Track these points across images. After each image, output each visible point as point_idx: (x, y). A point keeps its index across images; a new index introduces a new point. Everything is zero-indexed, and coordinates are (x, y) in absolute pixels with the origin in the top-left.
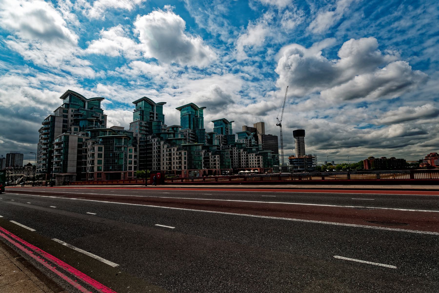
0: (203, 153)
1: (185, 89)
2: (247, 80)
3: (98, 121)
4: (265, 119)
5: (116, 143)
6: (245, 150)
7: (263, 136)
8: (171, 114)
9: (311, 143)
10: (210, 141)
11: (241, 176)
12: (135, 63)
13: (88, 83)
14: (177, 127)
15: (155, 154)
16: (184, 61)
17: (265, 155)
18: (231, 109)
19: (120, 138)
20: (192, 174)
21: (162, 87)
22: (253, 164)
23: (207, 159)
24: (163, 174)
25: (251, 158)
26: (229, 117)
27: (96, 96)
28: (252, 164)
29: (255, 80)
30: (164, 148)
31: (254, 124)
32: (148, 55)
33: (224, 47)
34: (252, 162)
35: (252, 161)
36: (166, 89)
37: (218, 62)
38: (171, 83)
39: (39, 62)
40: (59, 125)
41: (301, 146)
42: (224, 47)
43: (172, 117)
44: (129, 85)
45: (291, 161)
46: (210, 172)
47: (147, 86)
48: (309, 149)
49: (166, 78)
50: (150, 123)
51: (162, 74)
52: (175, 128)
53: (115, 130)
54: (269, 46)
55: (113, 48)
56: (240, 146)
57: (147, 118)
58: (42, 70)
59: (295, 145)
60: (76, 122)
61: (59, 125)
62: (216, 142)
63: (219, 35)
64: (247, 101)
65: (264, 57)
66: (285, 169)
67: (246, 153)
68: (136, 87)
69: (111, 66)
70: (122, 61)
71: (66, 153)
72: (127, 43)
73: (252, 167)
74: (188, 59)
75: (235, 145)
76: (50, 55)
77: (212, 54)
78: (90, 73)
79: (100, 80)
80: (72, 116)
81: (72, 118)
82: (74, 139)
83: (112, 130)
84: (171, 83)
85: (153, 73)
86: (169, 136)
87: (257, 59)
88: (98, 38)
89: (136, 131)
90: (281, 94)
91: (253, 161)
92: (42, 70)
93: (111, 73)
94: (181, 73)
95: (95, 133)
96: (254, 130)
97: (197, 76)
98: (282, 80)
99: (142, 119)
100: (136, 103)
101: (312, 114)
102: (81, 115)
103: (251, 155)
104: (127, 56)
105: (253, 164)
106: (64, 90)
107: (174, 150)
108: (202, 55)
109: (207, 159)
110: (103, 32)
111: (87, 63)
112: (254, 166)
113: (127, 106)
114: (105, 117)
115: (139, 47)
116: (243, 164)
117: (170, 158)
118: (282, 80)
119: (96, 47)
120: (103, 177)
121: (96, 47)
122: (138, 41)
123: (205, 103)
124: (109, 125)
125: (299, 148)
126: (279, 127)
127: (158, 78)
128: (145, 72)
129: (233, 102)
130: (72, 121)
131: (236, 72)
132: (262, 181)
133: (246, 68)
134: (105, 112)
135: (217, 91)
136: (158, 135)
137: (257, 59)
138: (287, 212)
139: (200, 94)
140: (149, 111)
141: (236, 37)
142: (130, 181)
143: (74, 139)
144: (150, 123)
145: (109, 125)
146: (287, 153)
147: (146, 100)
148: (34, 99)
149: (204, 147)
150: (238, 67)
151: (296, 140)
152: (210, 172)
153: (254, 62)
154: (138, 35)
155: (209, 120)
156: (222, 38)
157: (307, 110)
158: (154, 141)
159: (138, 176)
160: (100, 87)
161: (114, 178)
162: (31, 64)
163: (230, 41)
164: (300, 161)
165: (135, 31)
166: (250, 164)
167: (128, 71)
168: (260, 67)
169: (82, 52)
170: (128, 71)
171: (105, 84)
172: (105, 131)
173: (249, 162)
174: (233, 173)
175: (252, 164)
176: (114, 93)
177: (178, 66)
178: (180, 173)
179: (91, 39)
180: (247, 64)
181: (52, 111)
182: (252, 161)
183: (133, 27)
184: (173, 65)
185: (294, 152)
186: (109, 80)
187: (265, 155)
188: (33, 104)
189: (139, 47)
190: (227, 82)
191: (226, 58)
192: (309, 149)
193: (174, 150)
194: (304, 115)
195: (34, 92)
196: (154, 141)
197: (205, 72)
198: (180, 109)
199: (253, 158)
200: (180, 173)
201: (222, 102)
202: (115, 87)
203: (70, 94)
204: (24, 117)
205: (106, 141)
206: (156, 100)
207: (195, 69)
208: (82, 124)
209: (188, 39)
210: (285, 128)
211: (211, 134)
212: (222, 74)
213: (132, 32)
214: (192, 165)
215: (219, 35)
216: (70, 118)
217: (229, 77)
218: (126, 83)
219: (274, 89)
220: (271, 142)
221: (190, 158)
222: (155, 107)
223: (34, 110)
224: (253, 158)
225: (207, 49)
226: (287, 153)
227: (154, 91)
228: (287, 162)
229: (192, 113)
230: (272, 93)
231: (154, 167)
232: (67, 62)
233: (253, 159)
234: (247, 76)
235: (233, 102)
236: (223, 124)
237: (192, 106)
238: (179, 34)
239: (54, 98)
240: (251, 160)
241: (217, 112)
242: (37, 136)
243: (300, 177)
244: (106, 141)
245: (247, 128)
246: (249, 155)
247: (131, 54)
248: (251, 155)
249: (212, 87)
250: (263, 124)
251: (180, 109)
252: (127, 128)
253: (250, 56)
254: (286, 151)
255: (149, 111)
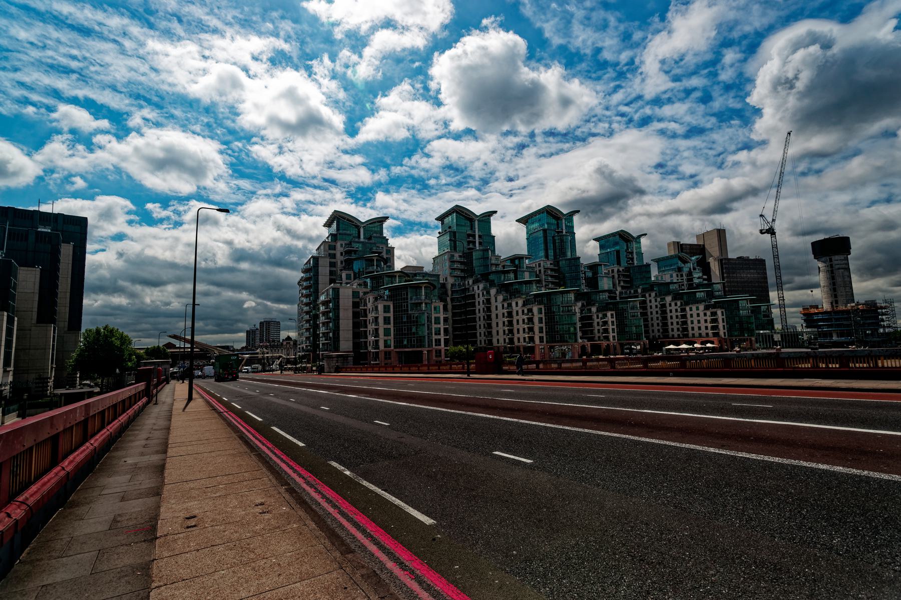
0: (577, 308)
1: (531, 178)
2: (674, 136)
3: (381, 259)
4: (725, 220)
5: (412, 299)
6: (677, 296)
7: (724, 262)
8: (508, 235)
9: (872, 271)
10: (593, 282)
11: (670, 356)
12: (436, 144)
13: (362, 194)
14: (520, 258)
15: (480, 315)
16: (528, 122)
17: (731, 308)
18: (636, 207)
19: (417, 287)
20: (557, 353)
21: (485, 182)
22: (700, 328)
23: (586, 320)
24: (498, 353)
25: (695, 315)
26: (633, 227)
27: (374, 214)
28: (696, 329)
29: (694, 132)
30: (498, 301)
31: (698, 236)
32: (458, 124)
33: (611, 73)
34: (696, 325)
35: (695, 322)
36: (495, 185)
37: (599, 111)
38: (503, 170)
39: (293, 171)
40: (324, 270)
41: (839, 280)
42: (611, 73)
43: (509, 238)
44: (426, 187)
45: (810, 318)
46: (596, 349)
47: (459, 185)
48: (863, 287)
49: (493, 163)
50: (468, 256)
51: (486, 156)
52: (517, 260)
53: (410, 273)
54: (727, 43)
55: (397, 125)
56: (663, 288)
57: (462, 245)
58: (296, 183)
59: (821, 278)
60: (348, 264)
61: (324, 270)
62: (605, 284)
63: (598, 50)
64: (675, 185)
65: (715, 74)
66: (791, 338)
67: (679, 303)
68: (441, 188)
69: (395, 159)
70: (414, 145)
71: (337, 318)
72: (421, 109)
73: (697, 335)
74: (537, 116)
75: (651, 287)
76: (306, 157)
77: (585, 94)
78: (364, 177)
79: (378, 186)
80: (342, 254)
81: (342, 258)
82: (346, 294)
83: (403, 273)
84: (503, 170)
85: (468, 158)
86: (507, 276)
87: (695, 82)
88: (372, 113)
89: (444, 272)
90: (773, 153)
91: (699, 322)
92: (296, 183)
93: (396, 170)
94: (522, 147)
95: (377, 281)
96: (699, 250)
97: (554, 147)
98: (771, 119)
99: (454, 247)
100: (441, 218)
101: (870, 192)
102: (355, 252)
103: (694, 308)
104: (422, 135)
105: (700, 328)
106: (328, 211)
107: (518, 305)
108: (566, 102)
109: (586, 320)
110: (382, 101)
111: (358, 159)
112: (704, 334)
113: (424, 227)
114: (391, 251)
115: (441, 112)
116: (674, 328)
117: (511, 320)
118: (771, 119)
119: (373, 129)
120: (394, 360)
121: (373, 129)
122: (438, 103)
123: (575, 202)
124: (399, 265)
125: (834, 284)
126: (767, 237)
127: (478, 165)
128: (454, 157)
129: (642, 192)
130: (342, 262)
131: (645, 122)
132: (727, 368)
133: (667, 110)
134: (392, 242)
135: (603, 172)
136: (485, 277)
137: (695, 82)
138: (679, 430)
139: (564, 184)
140: (466, 231)
141: (642, 44)
142: (438, 367)
143: (346, 294)
144: (468, 256)
145: (399, 265)
146: (795, 300)
147: (459, 212)
148: (290, 232)
149: (579, 296)
150: (648, 111)
151: (820, 265)
152: (596, 349)
153: (688, 92)
154: (438, 91)
155: (586, 237)
156: (607, 55)
157: (861, 182)
158: (478, 289)
159: (454, 356)
160: (381, 198)
161: (410, 361)
162: (283, 177)
163: (624, 57)
164: (837, 320)
165: (433, 85)
166: (693, 329)
167: (424, 163)
168: (706, 99)
169: (351, 142)
170: (424, 163)
171: (387, 191)
172: (392, 276)
173: (690, 326)
174: (649, 349)
175: (696, 329)
176: (404, 206)
177: (514, 133)
178: (531, 350)
179: (361, 119)
180: (670, 101)
181: (313, 249)
182: (695, 322)
183: (428, 78)
184: (506, 134)
185: (819, 296)
186: (394, 184)
187: (731, 308)
188: (288, 240)
189: (441, 112)
190: (624, 149)
191: (618, 97)
192: (863, 287)
193: (518, 305)
194: (845, 197)
195: (288, 221)
196: (478, 289)
197: (572, 138)
198: (524, 220)
199: (698, 315)
200: (531, 350)
201: (617, 195)
202: (404, 195)
203: (338, 218)
204: (278, 262)
205: (396, 293)
206: (478, 209)
207: (551, 133)
208: (357, 266)
209: (533, 75)
210: (784, 238)
211: (594, 267)
212: (611, 133)
213: (426, 89)
214: (554, 334)
215: (598, 50)
216: (339, 258)
217: (629, 137)
218: (421, 185)
219: (748, 146)
220: (750, 275)
221: (551, 319)
222: (476, 223)
223: (289, 250)
224: (698, 315)
225: (575, 87)
226: (795, 300)
227: (472, 192)
228: (797, 322)
229: (550, 226)
230: (743, 156)
231: (481, 339)
232: (330, 164)
233: (699, 317)
234: (673, 126)
235: (642, 192)
236: (620, 244)
237: (549, 211)
238: (516, 69)
239: (314, 228)
240: (695, 319)
241: (605, 217)
242: (296, 292)
243: (843, 359)
244: (396, 293)
245: (680, 247)
246: (688, 309)
247: (428, 130)
248: (694, 308)
249: (591, 165)
250: (721, 233)
251: (524, 220)
252: (428, 268)
253: (676, 79)
254: (790, 296)
255: (466, 231)
